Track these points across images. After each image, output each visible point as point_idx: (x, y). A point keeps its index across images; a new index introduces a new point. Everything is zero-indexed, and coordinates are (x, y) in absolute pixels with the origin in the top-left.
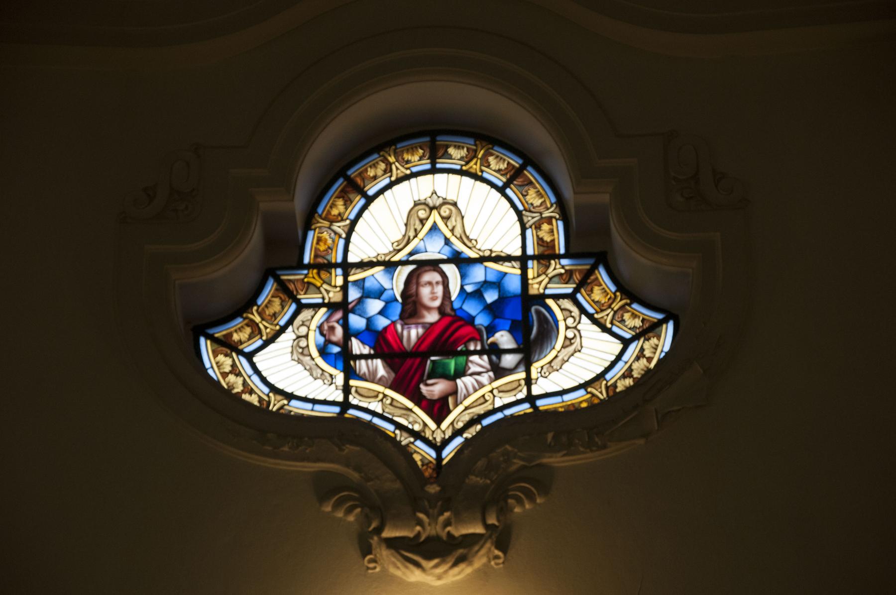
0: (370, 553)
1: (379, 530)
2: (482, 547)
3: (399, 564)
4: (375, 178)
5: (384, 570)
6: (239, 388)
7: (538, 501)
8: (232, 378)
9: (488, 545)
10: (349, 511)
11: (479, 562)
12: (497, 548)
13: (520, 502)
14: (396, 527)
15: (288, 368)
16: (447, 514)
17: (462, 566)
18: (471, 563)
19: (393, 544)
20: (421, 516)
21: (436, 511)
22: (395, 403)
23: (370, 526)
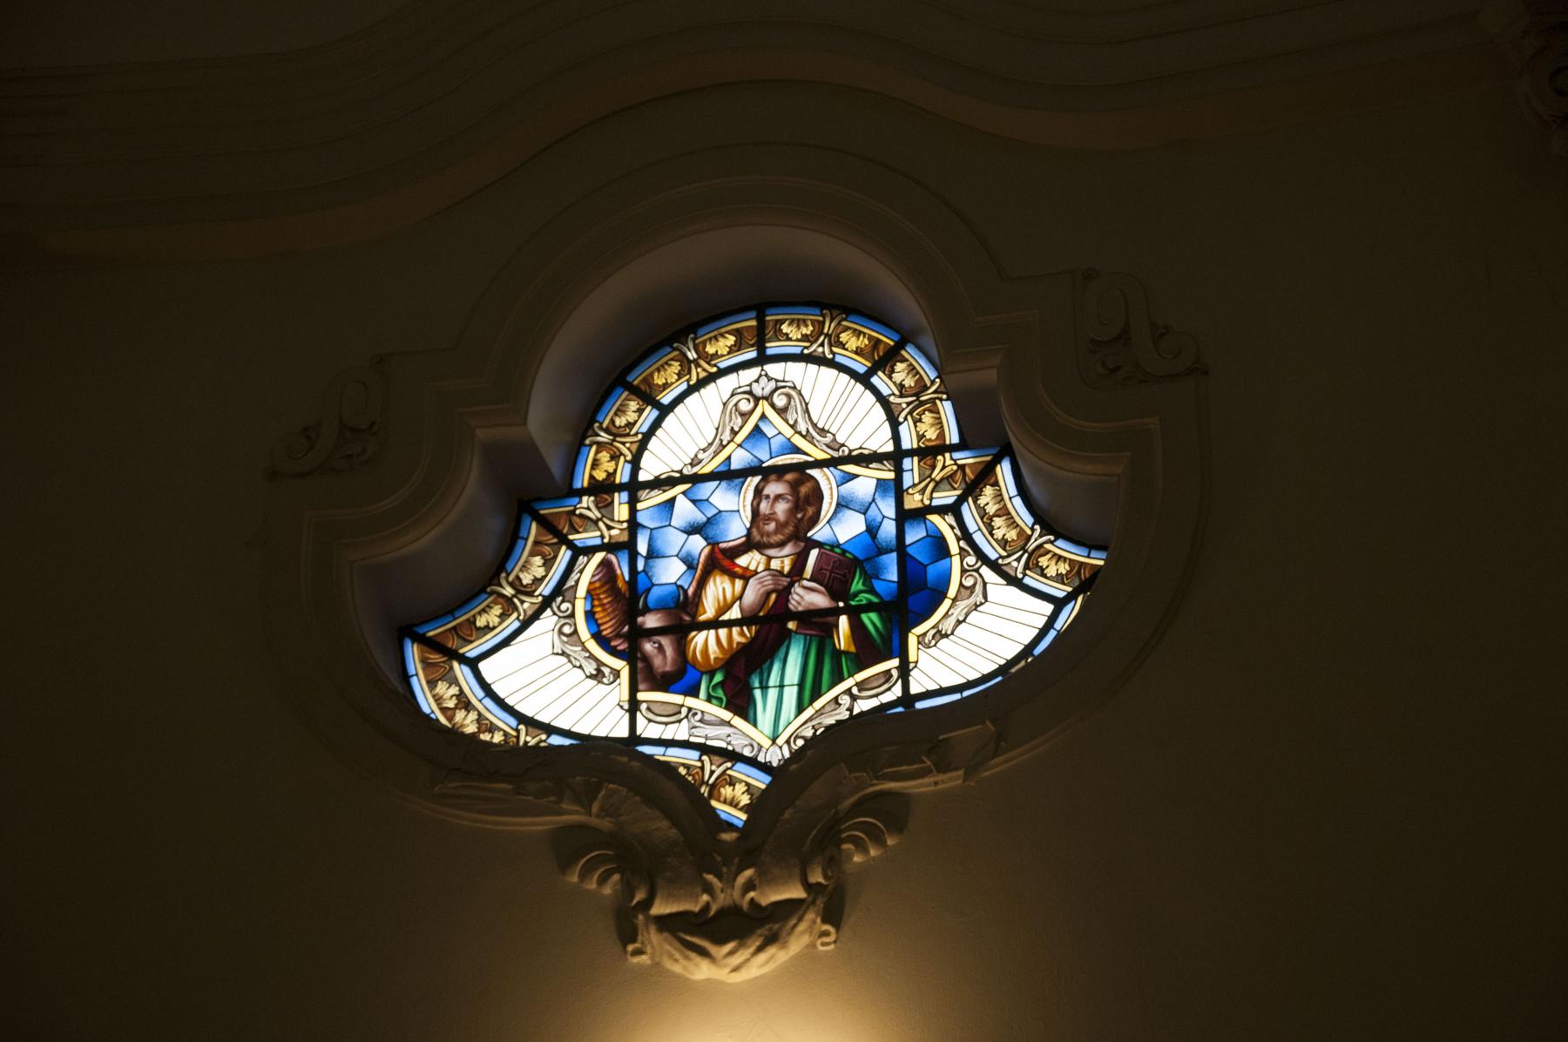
0: (634, 941)
1: (647, 904)
2: (800, 919)
3: (677, 956)
4: (666, 386)
5: (657, 964)
6: (471, 728)
7: (890, 842)
8: (460, 715)
9: (810, 916)
10: (603, 880)
11: (798, 942)
12: (824, 921)
13: (861, 846)
14: (671, 897)
15: (543, 678)
16: (749, 873)
17: (771, 950)
18: (784, 946)
19: (667, 924)
20: (710, 877)
21: (734, 868)
22: (707, 717)
23: (632, 898)
